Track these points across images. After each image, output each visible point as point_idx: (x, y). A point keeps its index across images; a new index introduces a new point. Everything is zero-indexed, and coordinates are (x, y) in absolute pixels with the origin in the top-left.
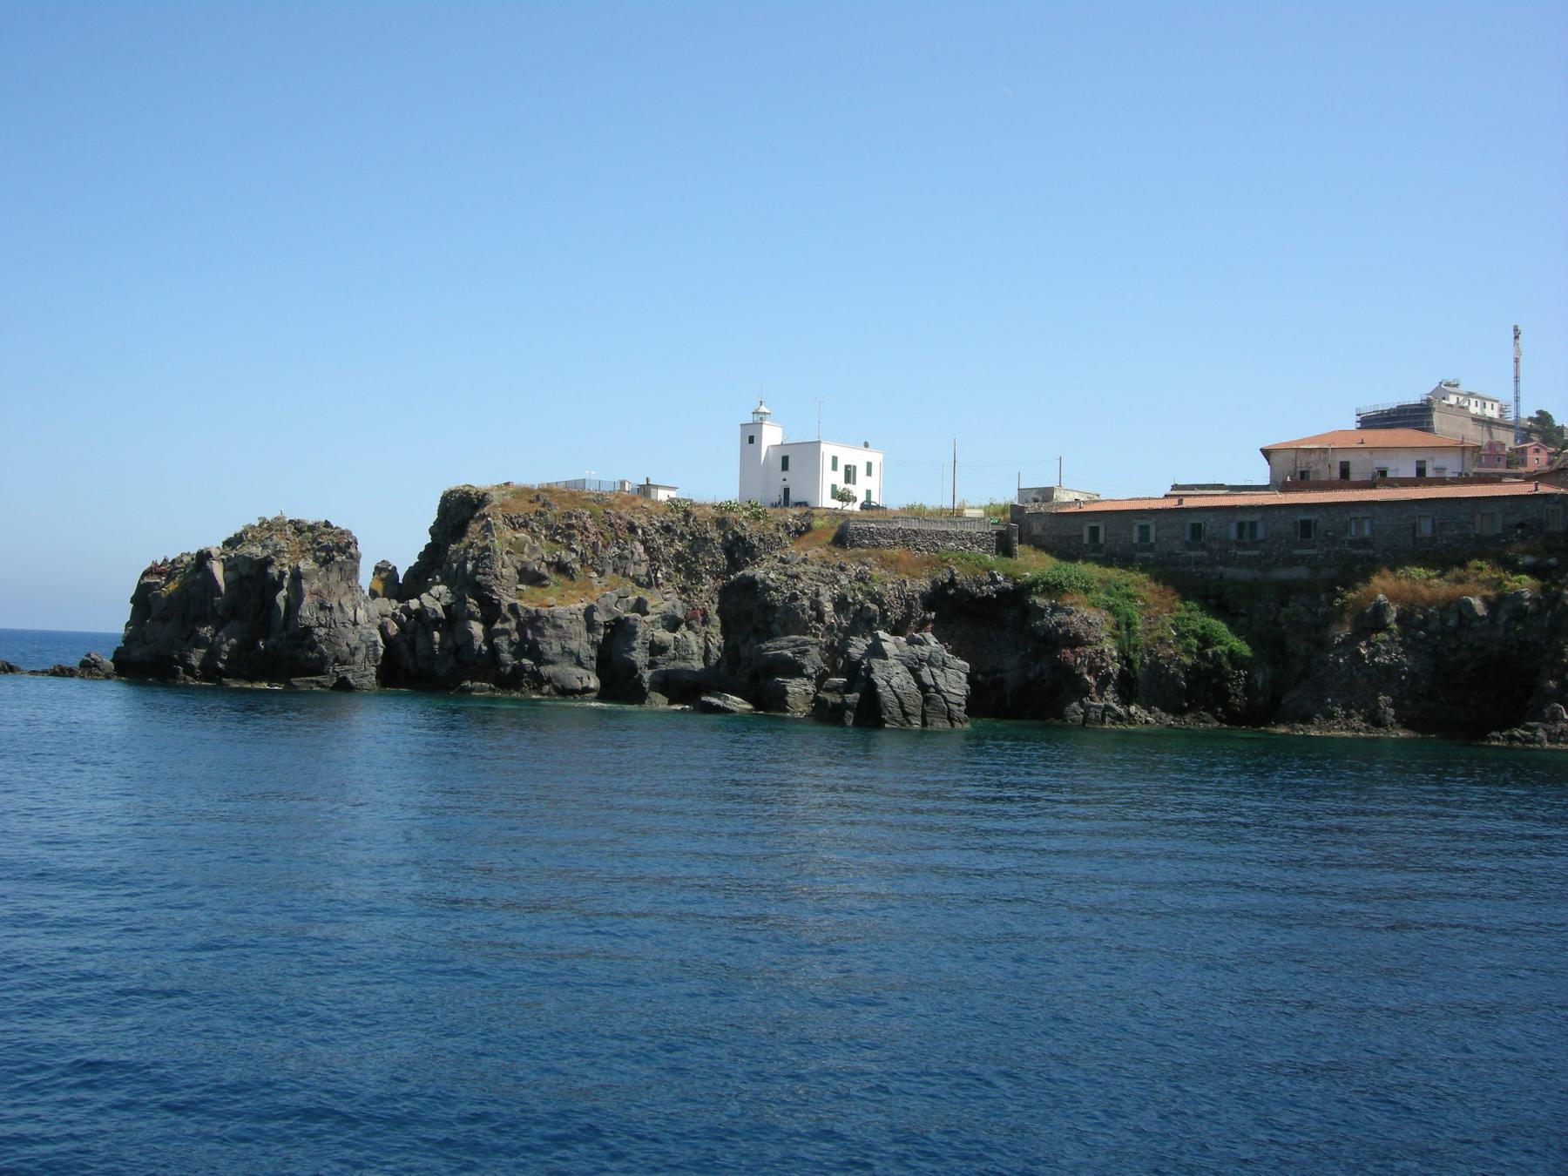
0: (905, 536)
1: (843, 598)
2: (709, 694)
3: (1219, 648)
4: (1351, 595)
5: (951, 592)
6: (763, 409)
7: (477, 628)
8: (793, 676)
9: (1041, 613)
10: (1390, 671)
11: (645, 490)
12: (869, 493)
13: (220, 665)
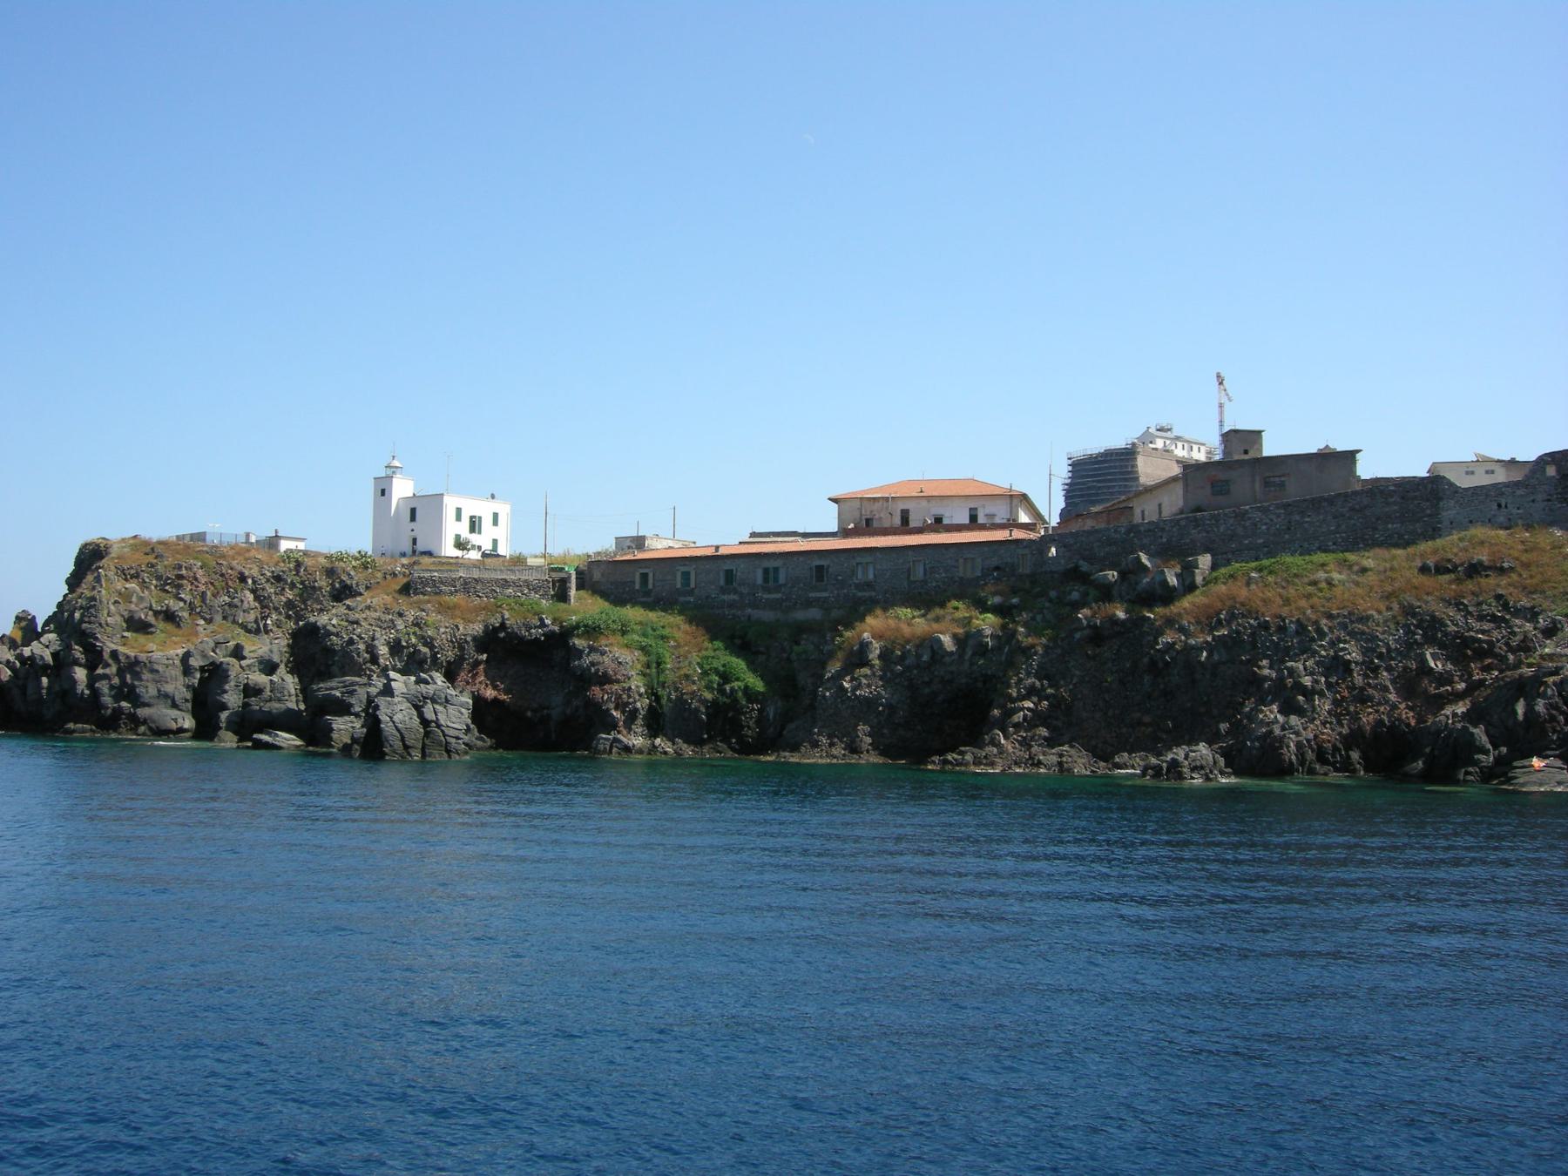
0: (466, 583)
1: (398, 642)
2: (261, 732)
3: (736, 684)
4: (848, 634)
5: (502, 635)
6: (396, 463)
7: (80, 674)
8: (341, 715)
9: (579, 653)
10: (870, 703)
11: (272, 542)
12: (495, 542)
13: (1520, 708)
